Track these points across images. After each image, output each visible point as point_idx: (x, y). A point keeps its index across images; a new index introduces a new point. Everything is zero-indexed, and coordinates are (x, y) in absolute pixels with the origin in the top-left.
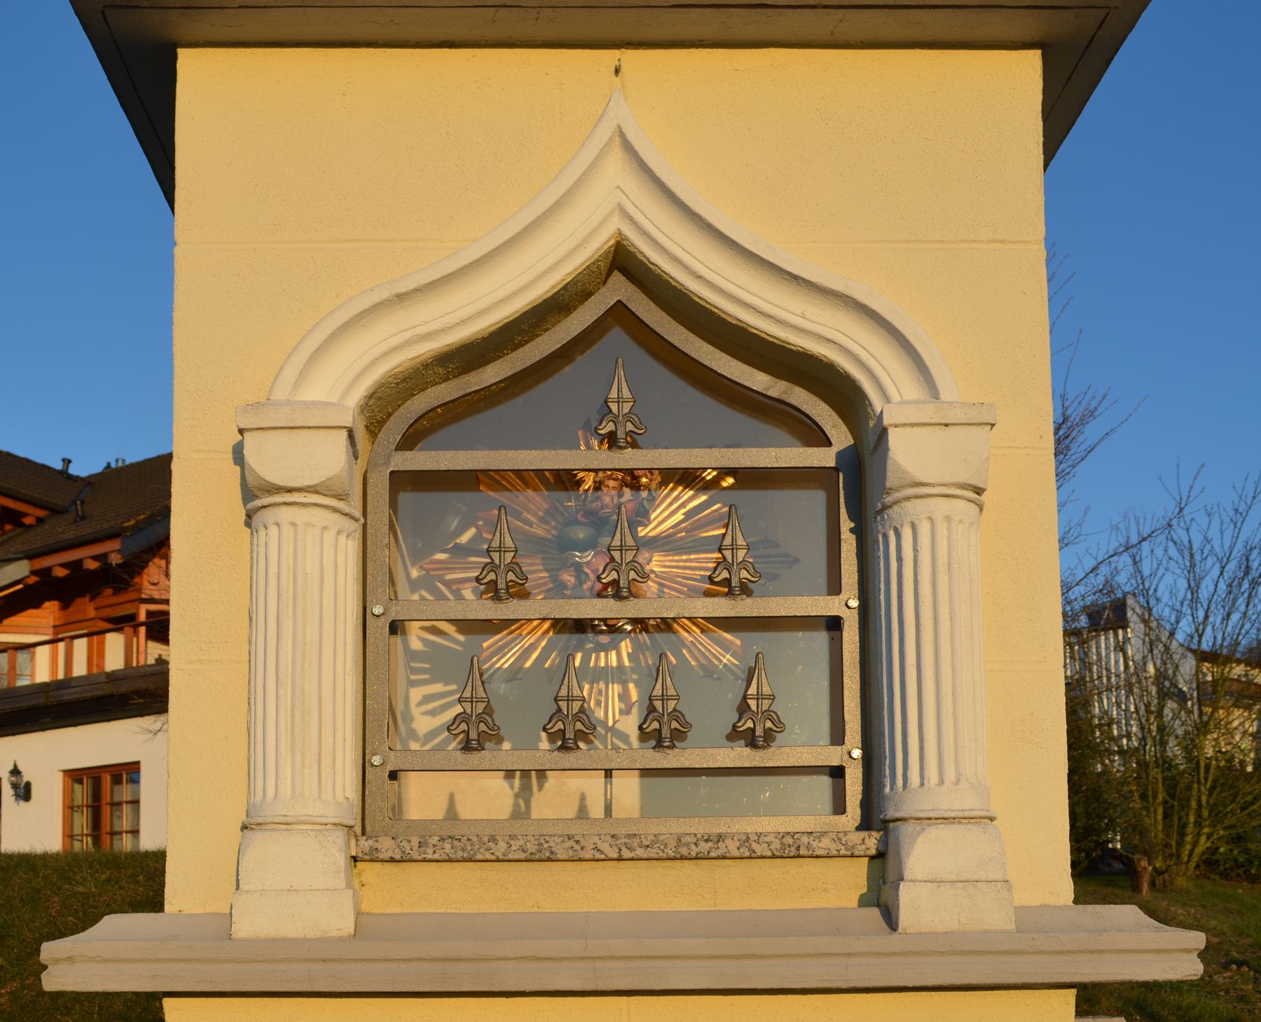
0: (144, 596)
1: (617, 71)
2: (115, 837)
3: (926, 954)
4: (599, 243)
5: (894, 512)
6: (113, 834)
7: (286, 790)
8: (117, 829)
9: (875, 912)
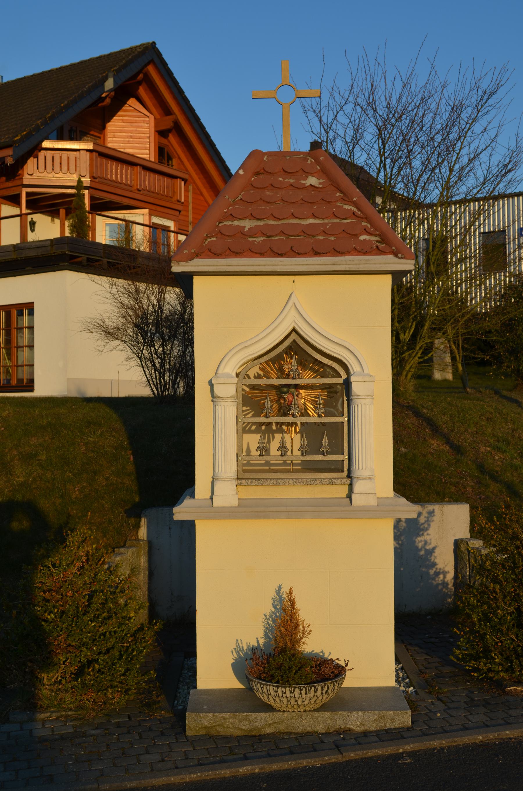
0: (24, 183)
1: (294, 282)
2: (19, 349)
3: (357, 511)
4: (291, 328)
5: (353, 400)
6: (18, 347)
7: (223, 471)
8: (20, 344)
9: (348, 499)
